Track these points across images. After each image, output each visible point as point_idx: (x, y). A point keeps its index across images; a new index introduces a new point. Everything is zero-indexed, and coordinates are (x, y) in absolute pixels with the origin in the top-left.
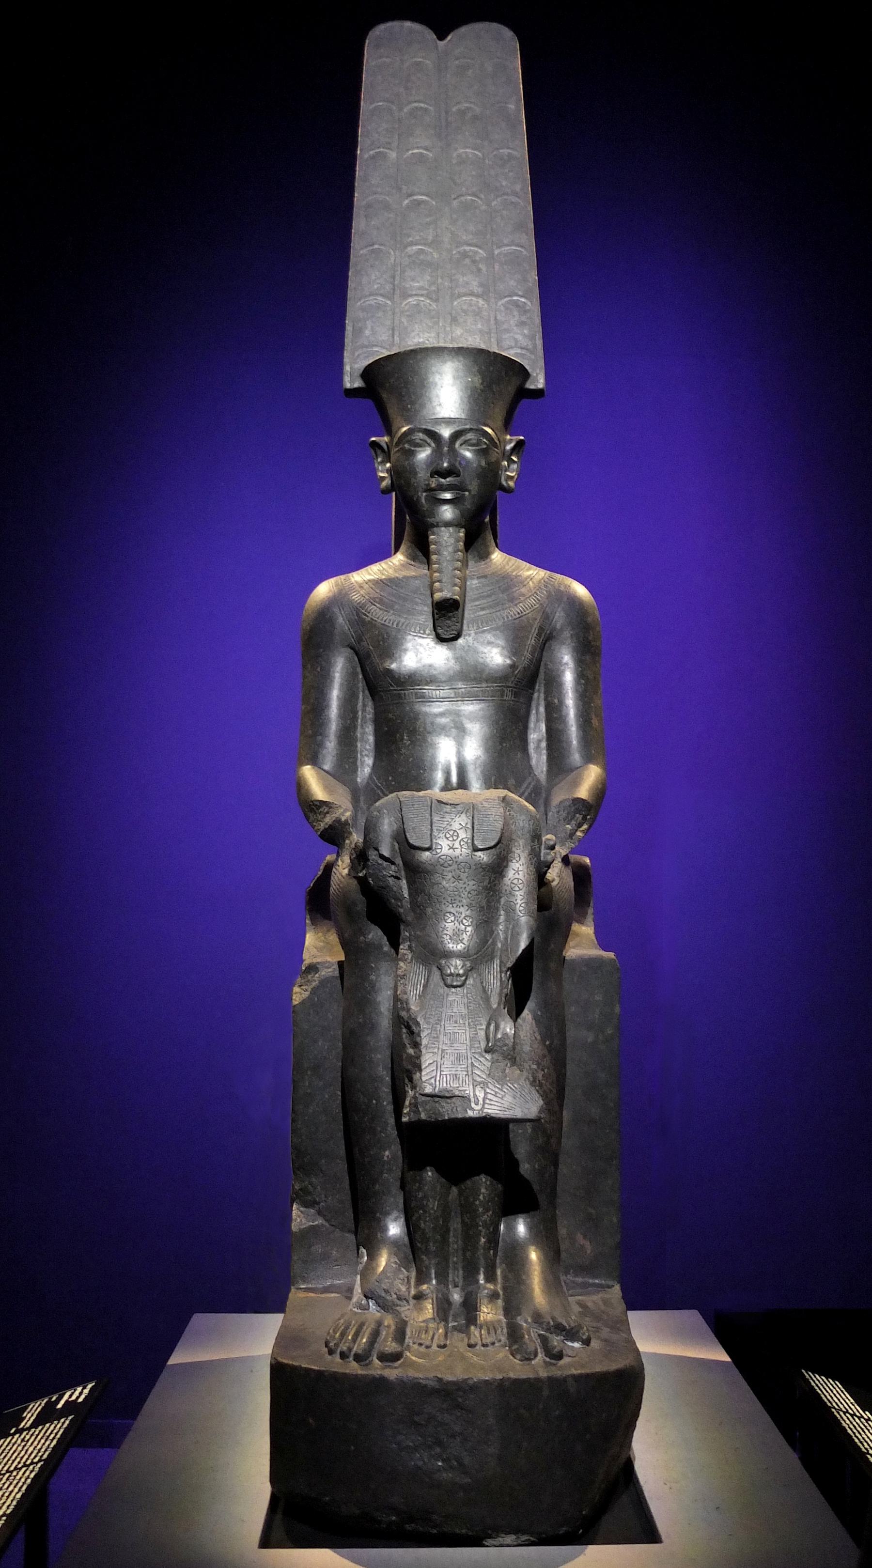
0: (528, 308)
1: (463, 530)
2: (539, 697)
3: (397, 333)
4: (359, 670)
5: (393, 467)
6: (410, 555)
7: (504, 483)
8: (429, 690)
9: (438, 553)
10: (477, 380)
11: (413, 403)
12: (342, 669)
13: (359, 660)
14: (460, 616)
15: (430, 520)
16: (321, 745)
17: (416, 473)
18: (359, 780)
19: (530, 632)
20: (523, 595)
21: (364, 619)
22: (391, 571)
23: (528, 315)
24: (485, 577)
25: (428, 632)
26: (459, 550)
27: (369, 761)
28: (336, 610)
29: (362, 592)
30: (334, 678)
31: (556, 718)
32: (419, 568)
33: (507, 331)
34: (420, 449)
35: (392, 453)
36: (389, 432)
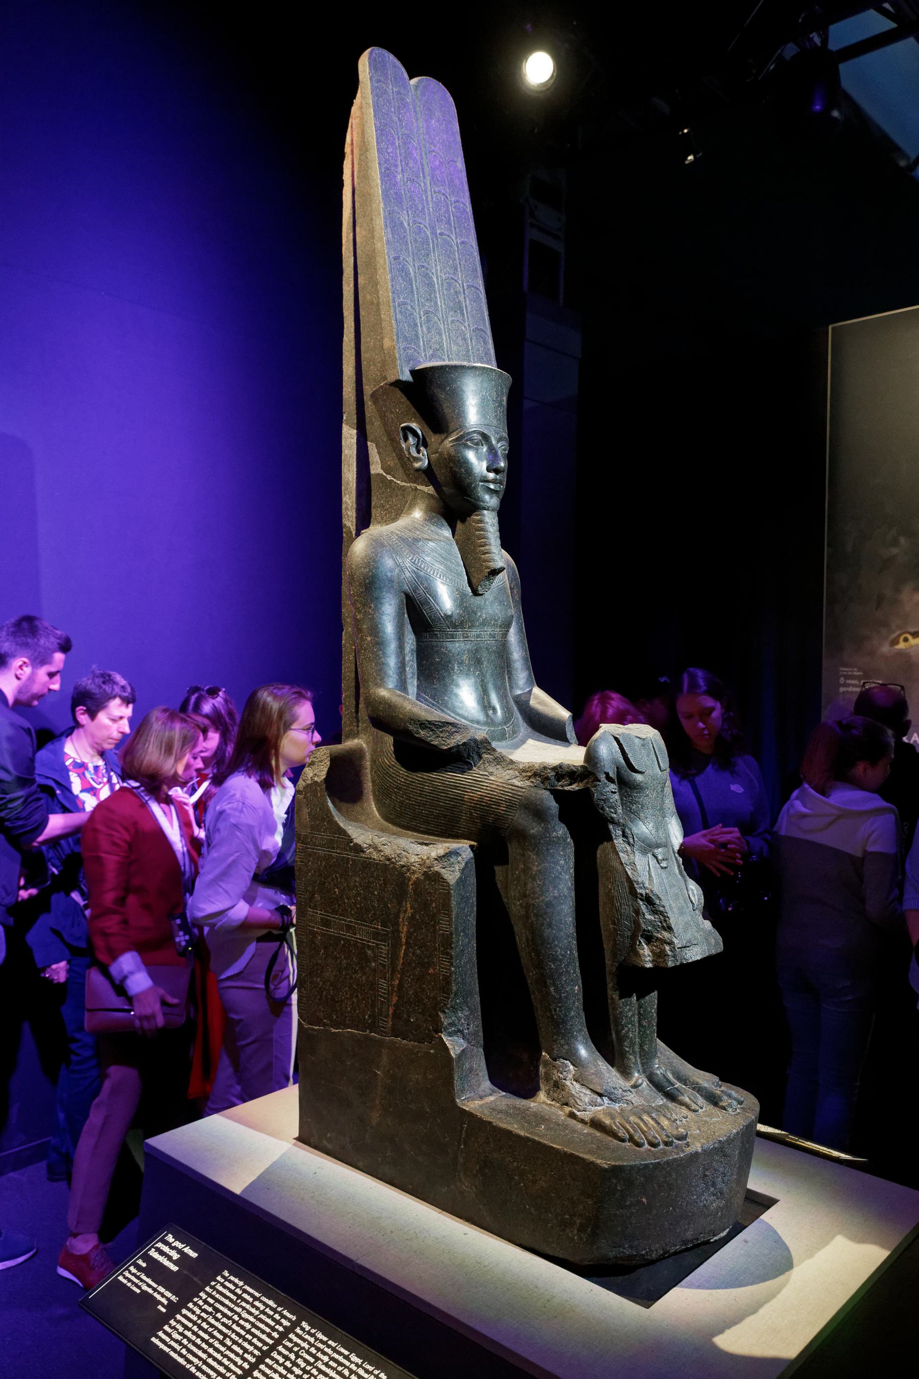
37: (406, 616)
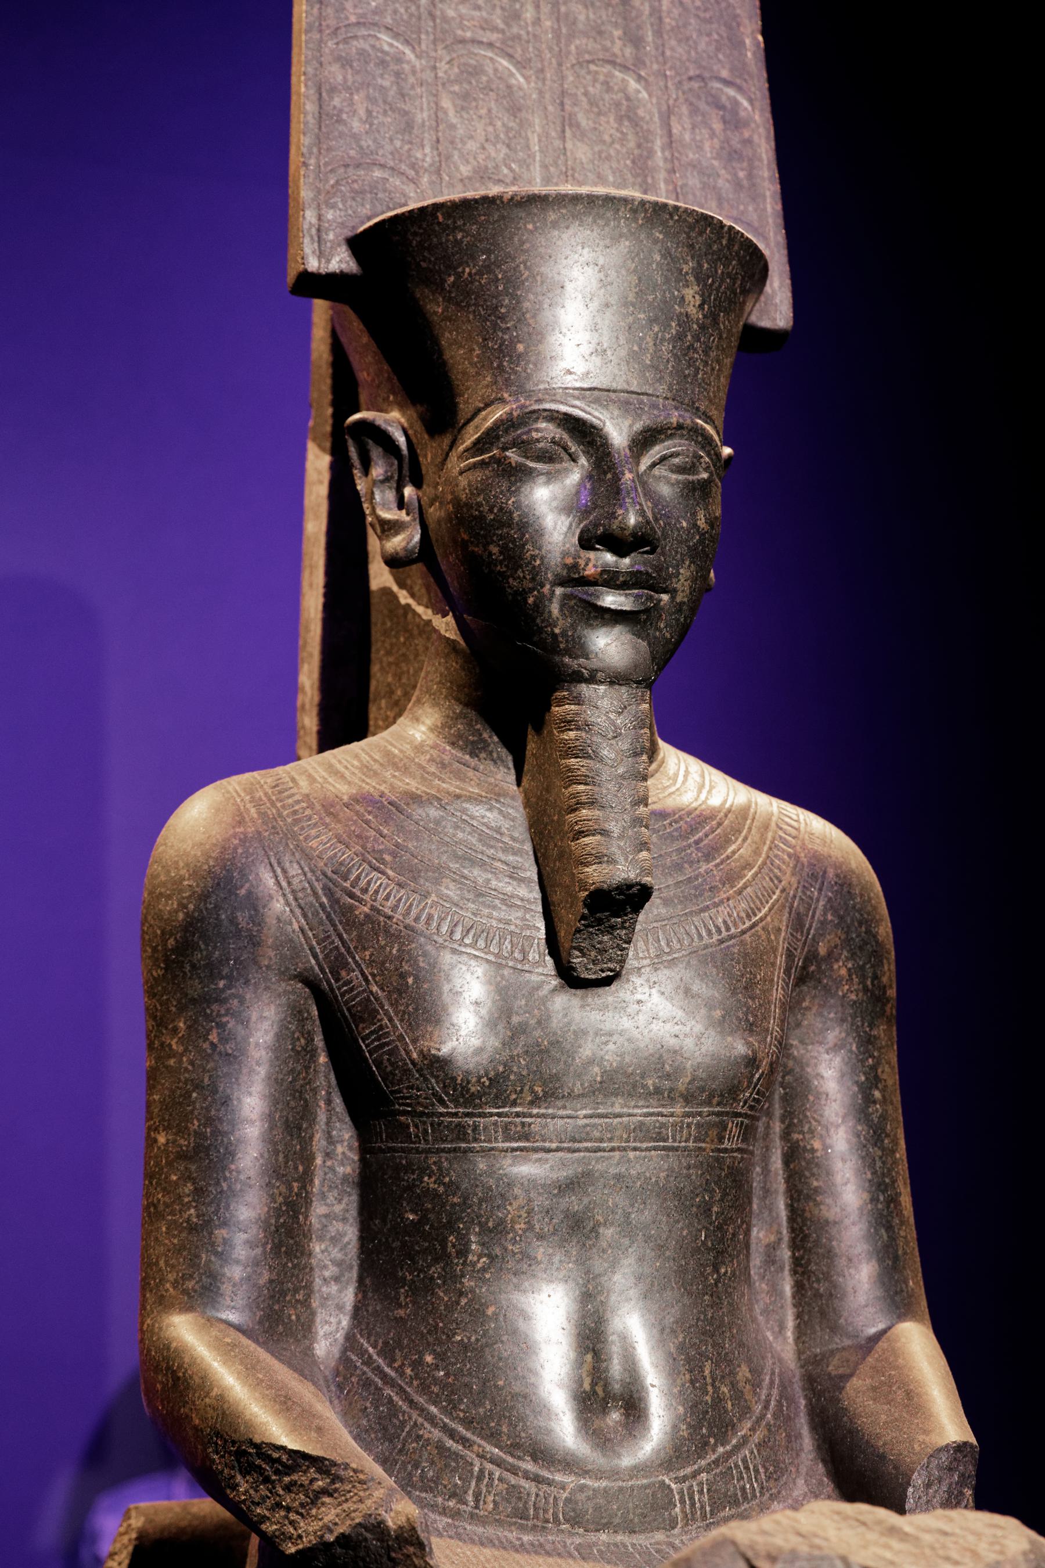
21: (351, 908)
37: (323, 1059)
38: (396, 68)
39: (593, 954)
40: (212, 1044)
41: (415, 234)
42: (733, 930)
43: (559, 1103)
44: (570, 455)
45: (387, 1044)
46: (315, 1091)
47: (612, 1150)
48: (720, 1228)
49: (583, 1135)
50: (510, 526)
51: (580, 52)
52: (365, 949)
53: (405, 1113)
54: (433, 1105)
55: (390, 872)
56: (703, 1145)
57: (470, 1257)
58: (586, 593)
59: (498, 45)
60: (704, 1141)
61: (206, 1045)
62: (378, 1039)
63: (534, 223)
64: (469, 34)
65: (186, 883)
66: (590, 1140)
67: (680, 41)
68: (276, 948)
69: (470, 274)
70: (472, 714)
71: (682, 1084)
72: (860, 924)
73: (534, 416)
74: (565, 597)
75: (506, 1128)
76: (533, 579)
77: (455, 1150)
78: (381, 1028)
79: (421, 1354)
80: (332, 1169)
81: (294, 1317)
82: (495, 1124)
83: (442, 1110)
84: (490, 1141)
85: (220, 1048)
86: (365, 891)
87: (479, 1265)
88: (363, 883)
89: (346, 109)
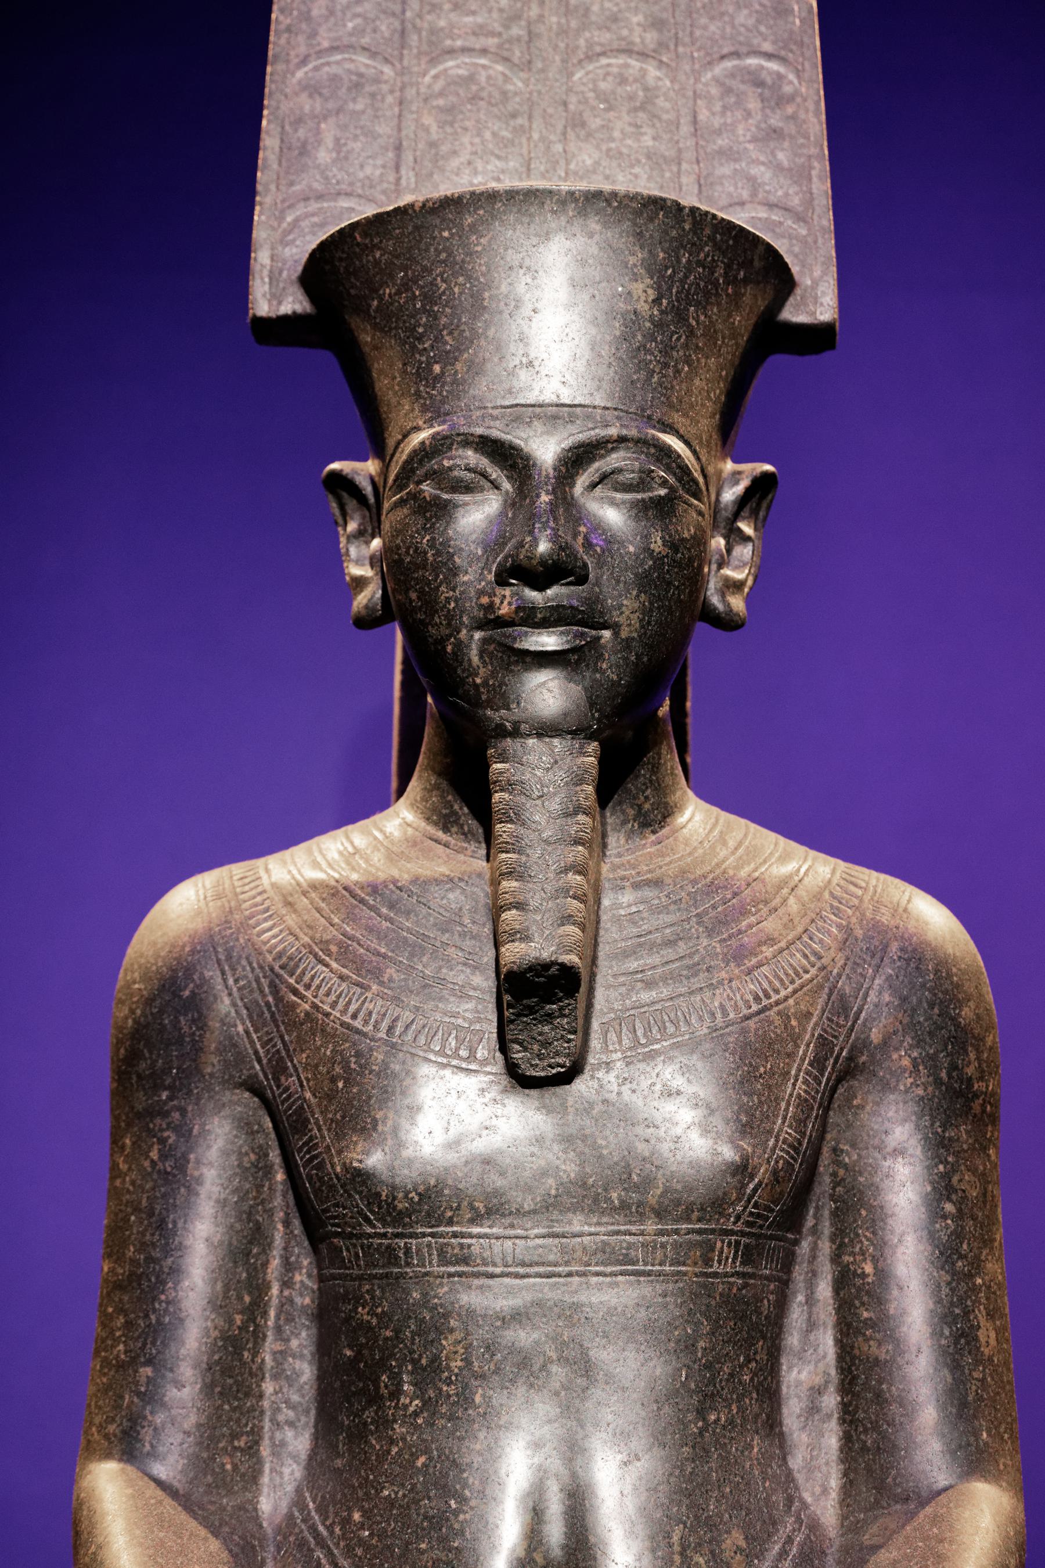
0: (787, 89)
1: (593, 746)
2: (814, 1248)
3: (408, 157)
4: (275, 1156)
5: (387, 549)
6: (434, 810)
7: (715, 600)
8: (488, 1240)
9: (515, 816)
10: (642, 292)
11: (448, 358)
12: (225, 1153)
13: (276, 1127)
14: (580, 1013)
15: (494, 716)
16: (151, 1396)
17: (454, 571)
18: (265, 1505)
19: (790, 1055)
20: (770, 941)
21: (293, 1006)
22: (377, 858)
23: (790, 110)
24: (657, 883)
25: (481, 1053)
26: (578, 810)
27: (299, 1442)
28: (212, 973)
29: (291, 920)
30: (199, 1181)
31: (870, 1323)
32: (461, 851)
33: (727, 154)
34: (467, 498)
35: (386, 505)
36: (377, 445)
38: (374, 88)
39: (536, 1047)
40: (152, 1161)
41: (341, 259)
42: (732, 1015)
43: (507, 1221)
44: (492, 482)
45: (316, 1157)
46: (270, 1212)
47: (570, 1275)
48: (708, 1366)
49: (536, 1258)
50: (424, 568)
51: (590, 45)
52: (302, 1051)
53: (337, 1235)
54: (360, 1225)
55: (334, 965)
56: (683, 1269)
57: (402, 1400)
58: (504, 635)
59: (492, 50)
60: (684, 1264)
61: (147, 1164)
62: (308, 1152)
63: (450, 230)
64: (459, 43)
65: (137, 986)
66: (543, 1264)
67: (712, 18)
68: (219, 1051)
69: (390, 295)
70: (445, 785)
71: (653, 1197)
72: (932, 1006)
73: (448, 442)
74: (485, 641)
75: (441, 1252)
76: (449, 625)
77: (387, 1276)
78: (311, 1139)
79: (350, 1510)
80: (291, 1301)
81: (229, 1467)
82: (429, 1245)
83: (369, 1230)
84: (424, 1266)
85: (160, 1166)
86: (308, 987)
87: (412, 1409)
88: (306, 979)
89: (311, 140)
